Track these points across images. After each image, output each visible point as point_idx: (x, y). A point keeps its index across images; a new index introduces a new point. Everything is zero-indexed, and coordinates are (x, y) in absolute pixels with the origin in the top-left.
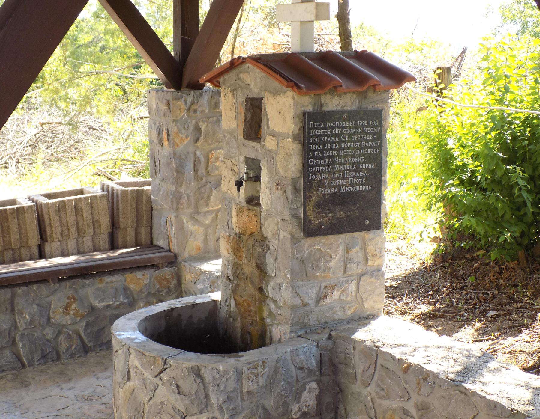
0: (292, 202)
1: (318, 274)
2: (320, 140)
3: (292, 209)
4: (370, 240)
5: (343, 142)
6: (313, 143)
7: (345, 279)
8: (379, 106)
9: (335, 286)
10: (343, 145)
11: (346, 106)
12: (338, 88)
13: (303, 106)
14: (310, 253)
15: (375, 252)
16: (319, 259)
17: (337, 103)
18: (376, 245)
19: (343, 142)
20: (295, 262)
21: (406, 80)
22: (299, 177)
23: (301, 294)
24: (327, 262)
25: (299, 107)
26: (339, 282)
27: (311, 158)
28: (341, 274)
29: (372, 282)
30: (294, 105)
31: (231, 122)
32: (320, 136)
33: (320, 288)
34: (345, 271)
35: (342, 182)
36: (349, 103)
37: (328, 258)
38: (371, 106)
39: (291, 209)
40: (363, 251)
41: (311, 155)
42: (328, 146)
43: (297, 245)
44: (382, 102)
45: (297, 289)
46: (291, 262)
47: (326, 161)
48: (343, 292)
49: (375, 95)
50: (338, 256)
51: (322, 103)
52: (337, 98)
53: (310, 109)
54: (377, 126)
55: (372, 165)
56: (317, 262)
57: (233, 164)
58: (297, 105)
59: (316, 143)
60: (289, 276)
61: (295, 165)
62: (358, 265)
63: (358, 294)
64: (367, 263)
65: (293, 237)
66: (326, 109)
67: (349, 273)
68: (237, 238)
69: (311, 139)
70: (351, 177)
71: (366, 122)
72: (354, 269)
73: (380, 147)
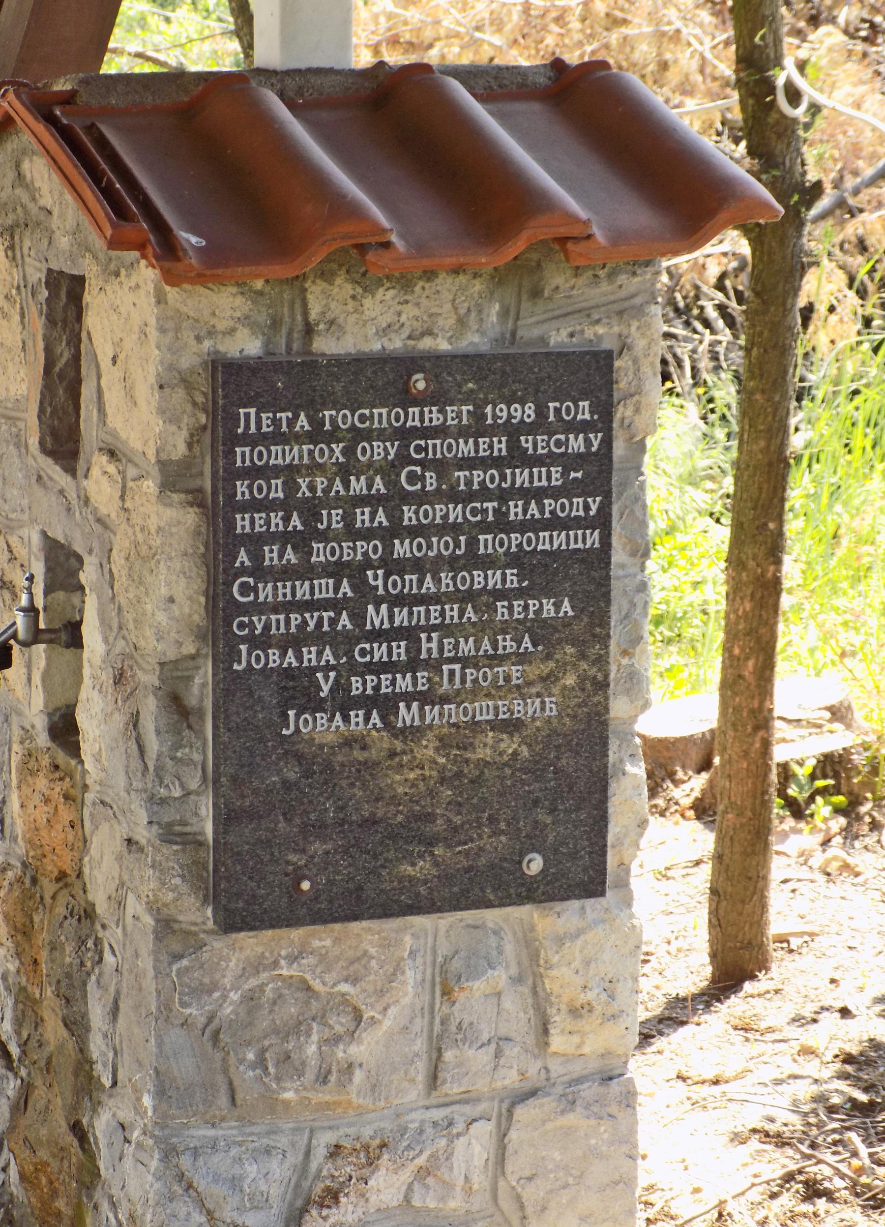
0: (159, 770)
1: (289, 1095)
2: (291, 487)
3: (163, 801)
4: (559, 941)
5: (406, 498)
6: (254, 506)
7: (437, 1114)
8: (602, 333)
9: (383, 1145)
10: (408, 514)
11: (429, 332)
12: (371, 256)
13: (212, 333)
14: (251, 999)
15: (583, 998)
16: (297, 1029)
17: (388, 318)
18: (587, 963)
19: (406, 498)
20: (176, 1036)
21: (722, 216)
22: (193, 657)
23: (201, 1184)
24: (337, 1039)
25: (188, 336)
26: (403, 1130)
27: (243, 571)
28: (414, 1093)
29: (568, 1131)
30: (162, 330)
31: (11, 369)
32: (290, 472)
33: (307, 1154)
34: (434, 1080)
35: (404, 683)
36: (447, 321)
37: (340, 1023)
38: (564, 333)
39: (155, 802)
40: (526, 990)
41: (243, 557)
42: (334, 519)
43: (185, 962)
44: (620, 313)
45: (185, 1162)
46: (159, 1037)
47: (324, 588)
48: (423, 1173)
49: (581, 281)
50: (392, 1011)
51: (313, 315)
52: (387, 295)
53: (249, 345)
54: (584, 427)
55: (558, 606)
56: (285, 1039)
57: (13, 559)
58: (178, 329)
59: (266, 506)
60: (147, 1101)
61: (171, 600)
62: (498, 1054)
63: (502, 1184)
64: (547, 1044)
65: (166, 926)
66: (326, 345)
67: (451, 1088)
68: (28, 881)
69: (241, 488)
70: (451, 661)
71: (530, 410)
72: (474, 1068)
73: (602, 522)
